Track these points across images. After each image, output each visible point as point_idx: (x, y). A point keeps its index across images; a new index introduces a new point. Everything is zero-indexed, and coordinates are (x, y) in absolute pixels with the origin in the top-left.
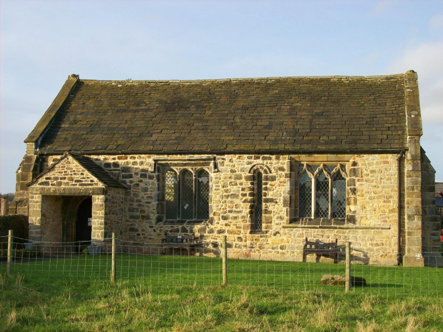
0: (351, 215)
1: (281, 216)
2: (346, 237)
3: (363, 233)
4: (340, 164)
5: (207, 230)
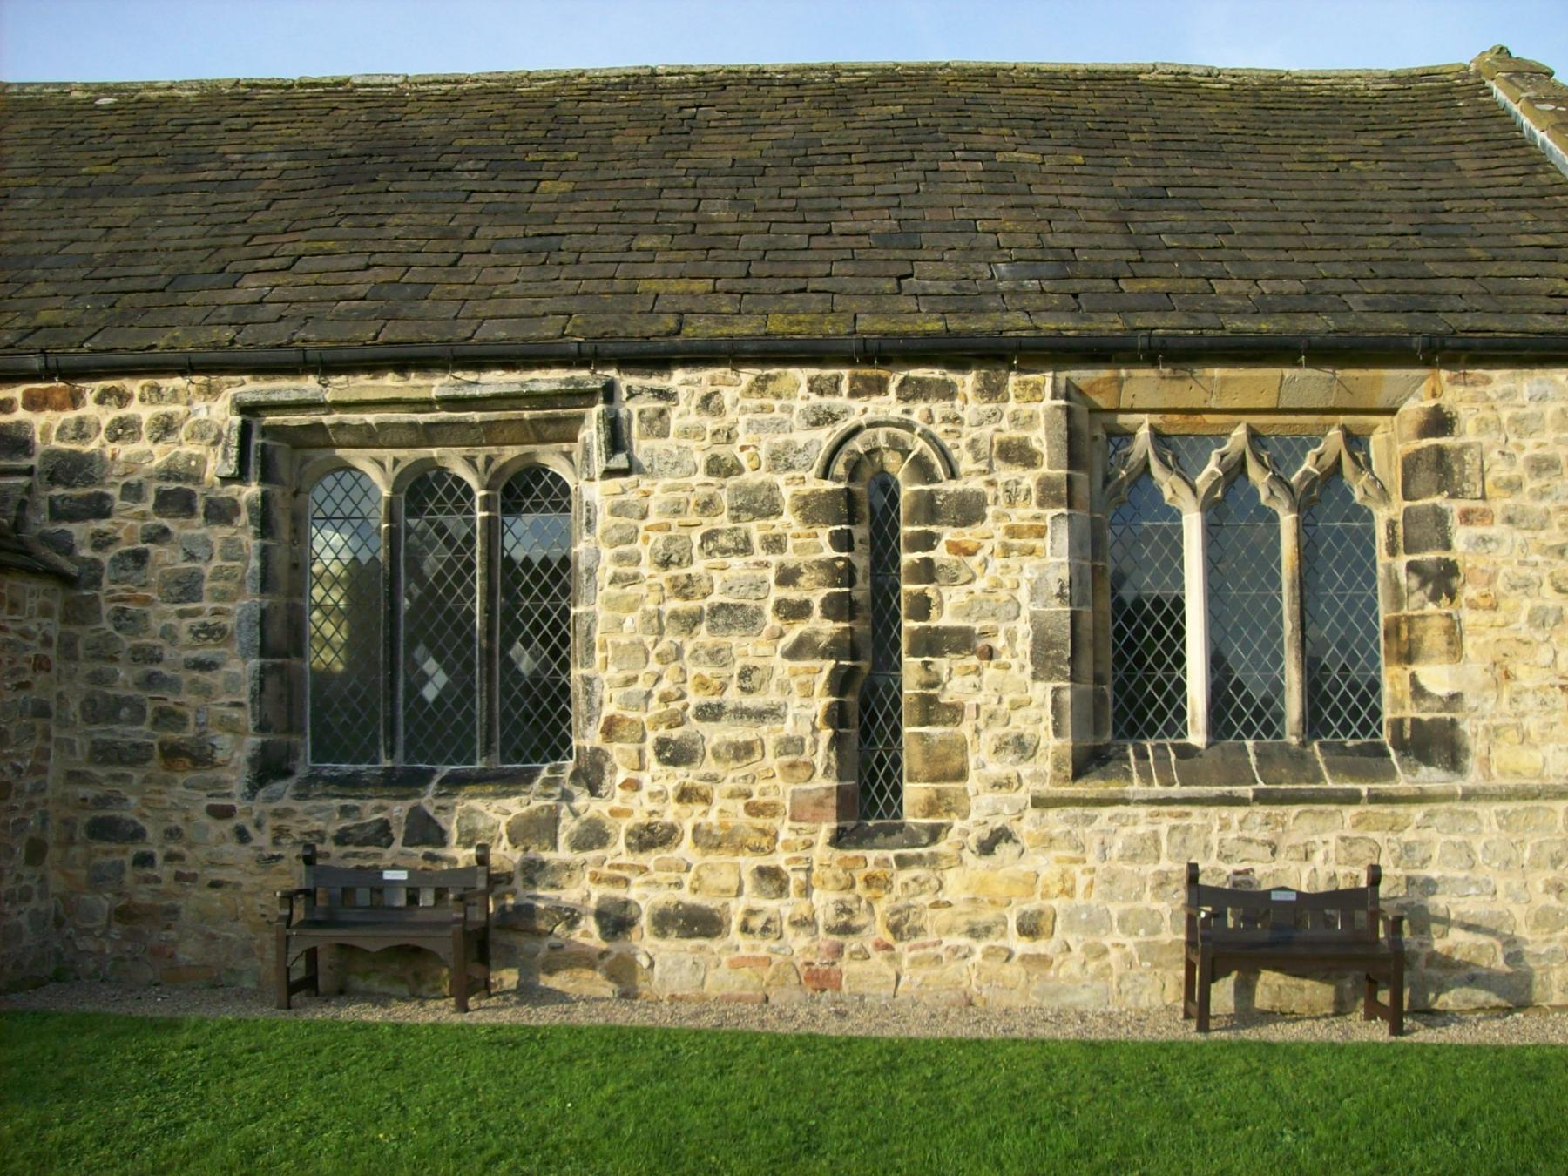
0: (1426, 717)
1: (1019, 737)
2: (1408, 848)
3: (1505, 821)
4: (1343, 428)
5: (568, 826)
